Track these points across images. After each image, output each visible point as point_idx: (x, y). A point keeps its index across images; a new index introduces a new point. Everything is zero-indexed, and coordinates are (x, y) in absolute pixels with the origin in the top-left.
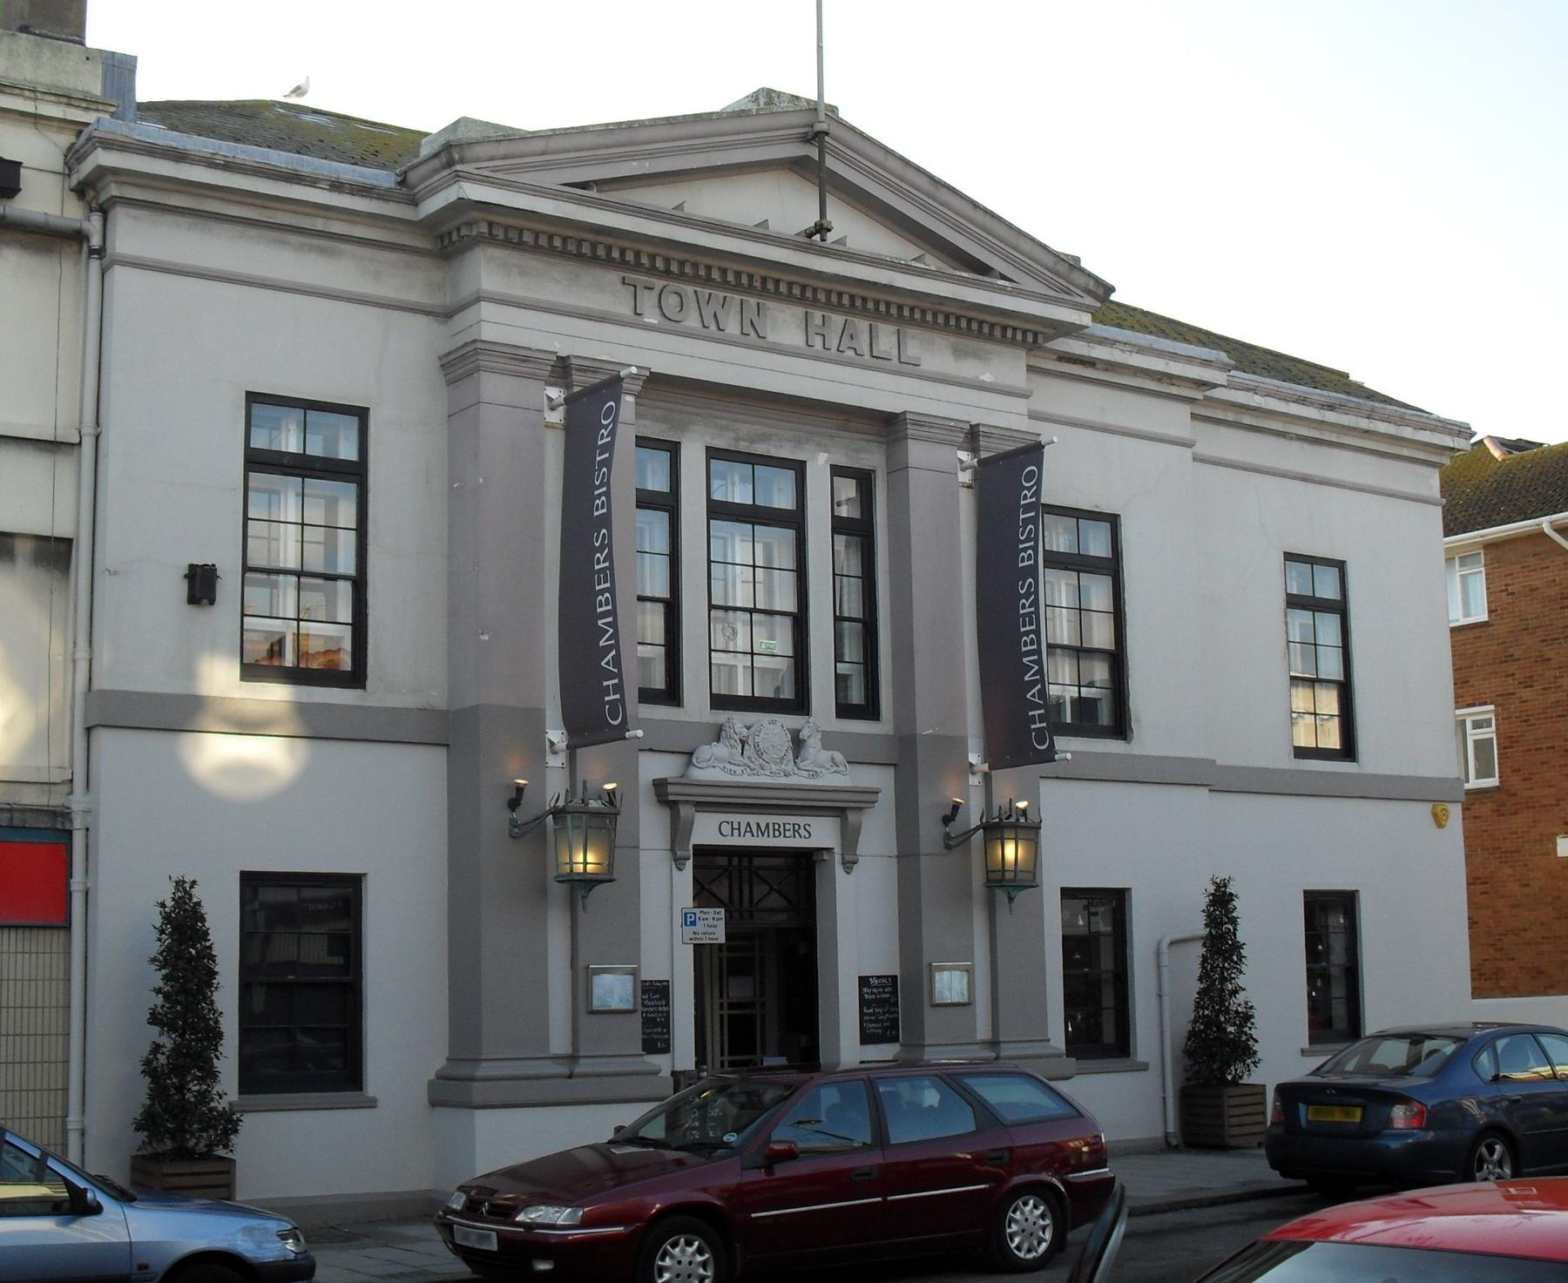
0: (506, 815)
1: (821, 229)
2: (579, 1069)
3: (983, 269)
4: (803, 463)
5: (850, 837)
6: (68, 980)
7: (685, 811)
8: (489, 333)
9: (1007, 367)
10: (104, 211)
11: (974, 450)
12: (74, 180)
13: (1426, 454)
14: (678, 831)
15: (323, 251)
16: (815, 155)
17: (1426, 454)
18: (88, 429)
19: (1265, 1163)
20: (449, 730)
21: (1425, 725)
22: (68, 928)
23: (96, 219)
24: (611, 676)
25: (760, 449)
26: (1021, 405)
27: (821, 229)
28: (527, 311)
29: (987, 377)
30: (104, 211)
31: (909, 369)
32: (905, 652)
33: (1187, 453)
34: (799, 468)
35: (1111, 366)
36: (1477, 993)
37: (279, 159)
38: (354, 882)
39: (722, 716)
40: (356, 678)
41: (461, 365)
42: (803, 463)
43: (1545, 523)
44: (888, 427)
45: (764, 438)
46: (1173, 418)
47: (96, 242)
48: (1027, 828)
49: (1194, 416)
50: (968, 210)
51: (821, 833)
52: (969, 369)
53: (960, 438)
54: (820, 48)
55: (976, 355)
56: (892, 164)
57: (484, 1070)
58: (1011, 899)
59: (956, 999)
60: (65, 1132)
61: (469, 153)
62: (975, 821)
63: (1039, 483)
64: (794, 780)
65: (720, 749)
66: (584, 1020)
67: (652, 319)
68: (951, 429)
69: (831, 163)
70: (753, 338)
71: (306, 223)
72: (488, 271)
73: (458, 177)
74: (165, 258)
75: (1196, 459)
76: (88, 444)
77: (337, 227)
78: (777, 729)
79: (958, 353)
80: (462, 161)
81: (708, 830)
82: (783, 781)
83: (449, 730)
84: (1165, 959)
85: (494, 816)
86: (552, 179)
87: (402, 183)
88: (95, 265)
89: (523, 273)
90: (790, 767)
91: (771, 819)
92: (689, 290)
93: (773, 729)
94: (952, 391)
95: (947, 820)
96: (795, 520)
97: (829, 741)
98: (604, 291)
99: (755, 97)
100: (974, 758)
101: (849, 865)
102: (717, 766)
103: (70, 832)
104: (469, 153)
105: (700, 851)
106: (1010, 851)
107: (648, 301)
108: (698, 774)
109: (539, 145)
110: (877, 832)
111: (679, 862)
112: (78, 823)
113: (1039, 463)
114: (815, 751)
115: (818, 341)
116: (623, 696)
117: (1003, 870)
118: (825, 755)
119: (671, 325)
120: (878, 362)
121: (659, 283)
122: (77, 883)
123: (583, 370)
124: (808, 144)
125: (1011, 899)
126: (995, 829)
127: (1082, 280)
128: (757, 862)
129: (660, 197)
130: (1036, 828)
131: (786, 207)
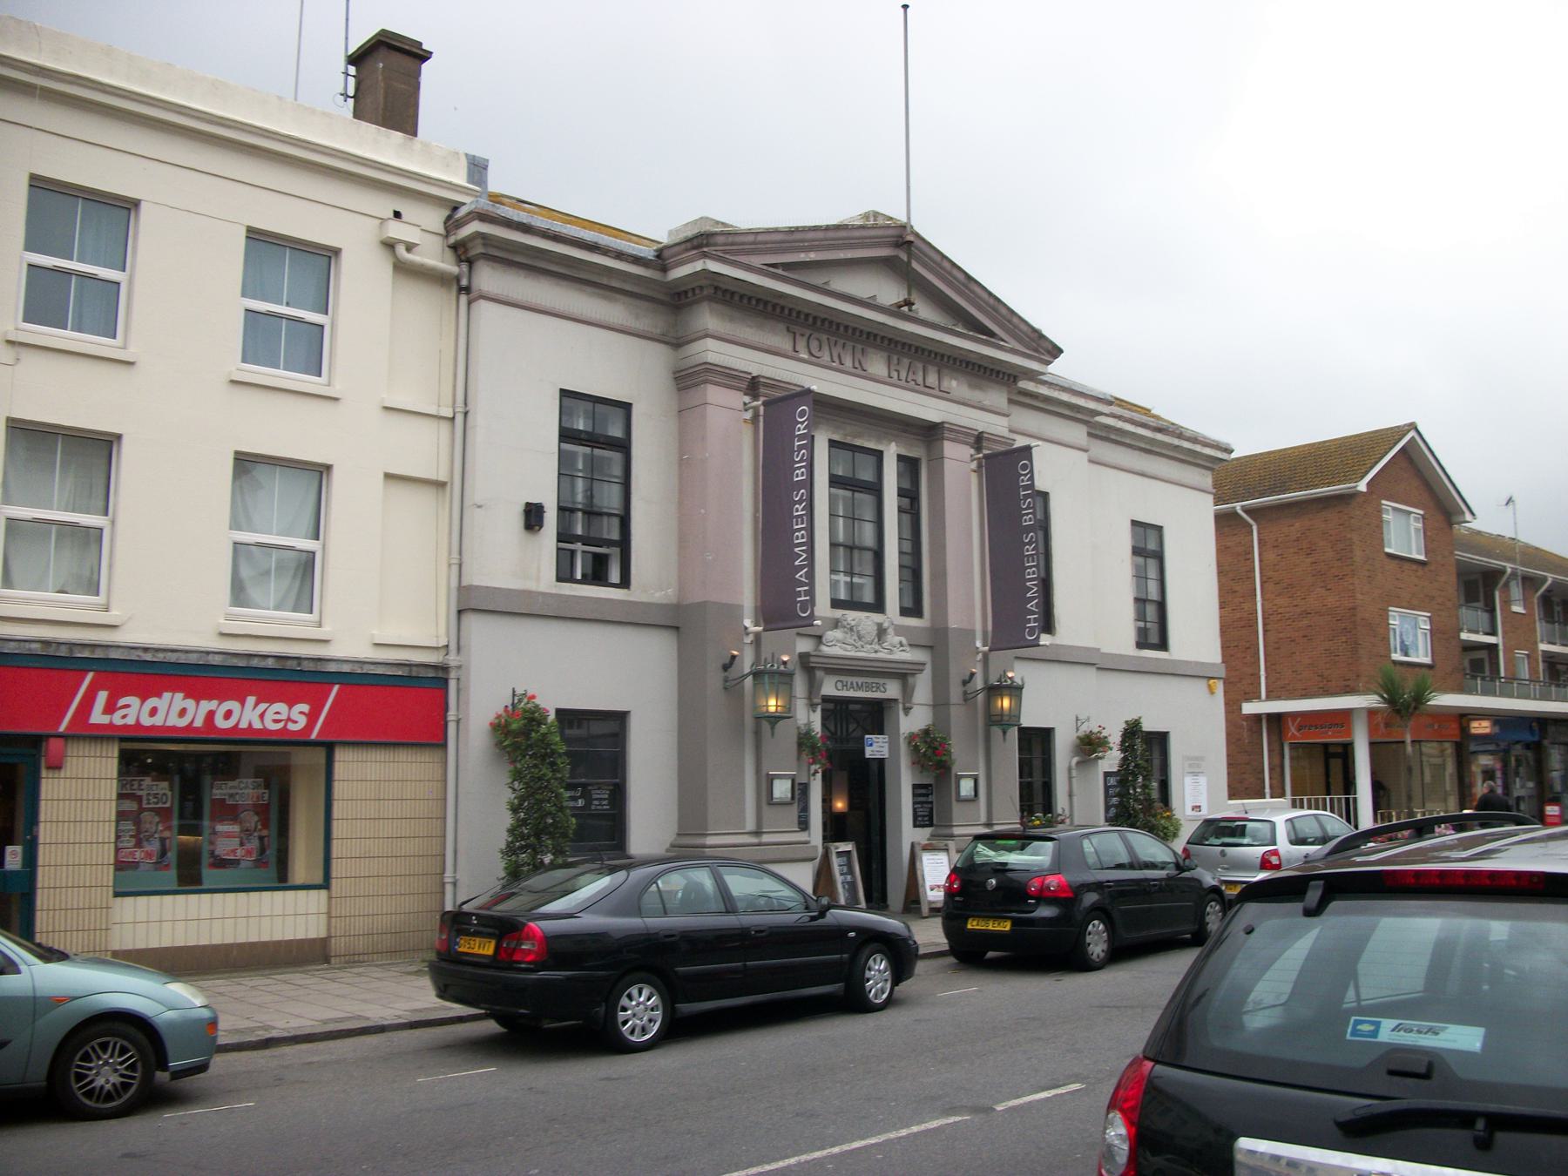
0: (722, 674)
1: (908, 303)
3: (991, 334)
4: (881, 453)
5: (907, 692)
6: (445, 781)
7: (819, 674)
8: (712, 358)
9: (997, 397)
10: (470, 263)
11: (979, 450)
12: (452, 240)
13: (1209, 464)
14: (813, 686)
15: (605, 298)
16: (904, 257)
17: (1209, 464)
18: (460, 408)
20: (677, 621)
21: (1196, 631)
22: (444, 746)
23: (465, 267)
24: (802, 584)
25: (858, 442)
26: (1004, 421)
27: (908, 303)
28: (725, 345)
29: (987, 403)
30: (470, 263)
31: (944, 395)
32: (940, 575)
33: (1085, 456)
34: (879, 455)
35: (1047, 399)
36: (1233, 794)
38: (621, 717)
39: (838, 613)
41: (688, 379)
42: (881, 453)
43: (1238, 506)
44: (930, 433)
45: (859, 436)
46: (1078, 433)
47: (464, 282)
48: (1015, 690)
49: (1090, 434)
50: (985, 296)
51: (892, 690)
53: (972, 440)
55: (980, 388)
56: (946, 265)
57: (710, 841)
58: (1004, 733)
60: (443, 884)
61: (712, 241)
62: (747, 670)
63: (1032, 471)
64: (881, 655)
66: (765, 808)
67: (805, 356)
68: (967, 434)
69: (915, 265)
70: (860, 372)
72: (708, 318)
73: (705, 255)
75: (1091, 461)
76: (459, 419)
77: (615, 284)
79: (972, 386)
80: (707, 245)
81: (830, 688)
82: (873, 655)
83: (677, 621)
84: (1074, 773)
85: (714, 679)
86: (757, 261)
87: (658, 256)
88: (464, 299)
89: (732, 319)
90: (877, 647)
92: (824, 337)
93: (866, 621)
94: (991, 416)
95: (726, 668)
96: (876, 489)
97: (900, 630)
99: (866, 216)
100: (748, 623)
101: (907, 710)
102: (836, 646)
103: (446, 681)
104: (712, 241)
105: (826, 699)
106: (1006, 703)
107: (801, 344)
108: (825, 650)
109: (751, 238)
110: (923, 689)
111: (812, 706)
112: (453, 675)
113: (1030, 459)
114: (892, 639)
115: (895, 374)
116: (578, 582)
117: (1002, 715)
118: (897, 639)
119: (814, 361)
120: (926, 390)
121: (808, 332)
122: (452, 715)
123: (766, 385)
124: (899, 250)
125: (1004, 733)
126: (994, 691)
127: (1047, 345)
128: (852, 707)
129: (817, 279)
130: (1020, 688)
131: (889, 292)
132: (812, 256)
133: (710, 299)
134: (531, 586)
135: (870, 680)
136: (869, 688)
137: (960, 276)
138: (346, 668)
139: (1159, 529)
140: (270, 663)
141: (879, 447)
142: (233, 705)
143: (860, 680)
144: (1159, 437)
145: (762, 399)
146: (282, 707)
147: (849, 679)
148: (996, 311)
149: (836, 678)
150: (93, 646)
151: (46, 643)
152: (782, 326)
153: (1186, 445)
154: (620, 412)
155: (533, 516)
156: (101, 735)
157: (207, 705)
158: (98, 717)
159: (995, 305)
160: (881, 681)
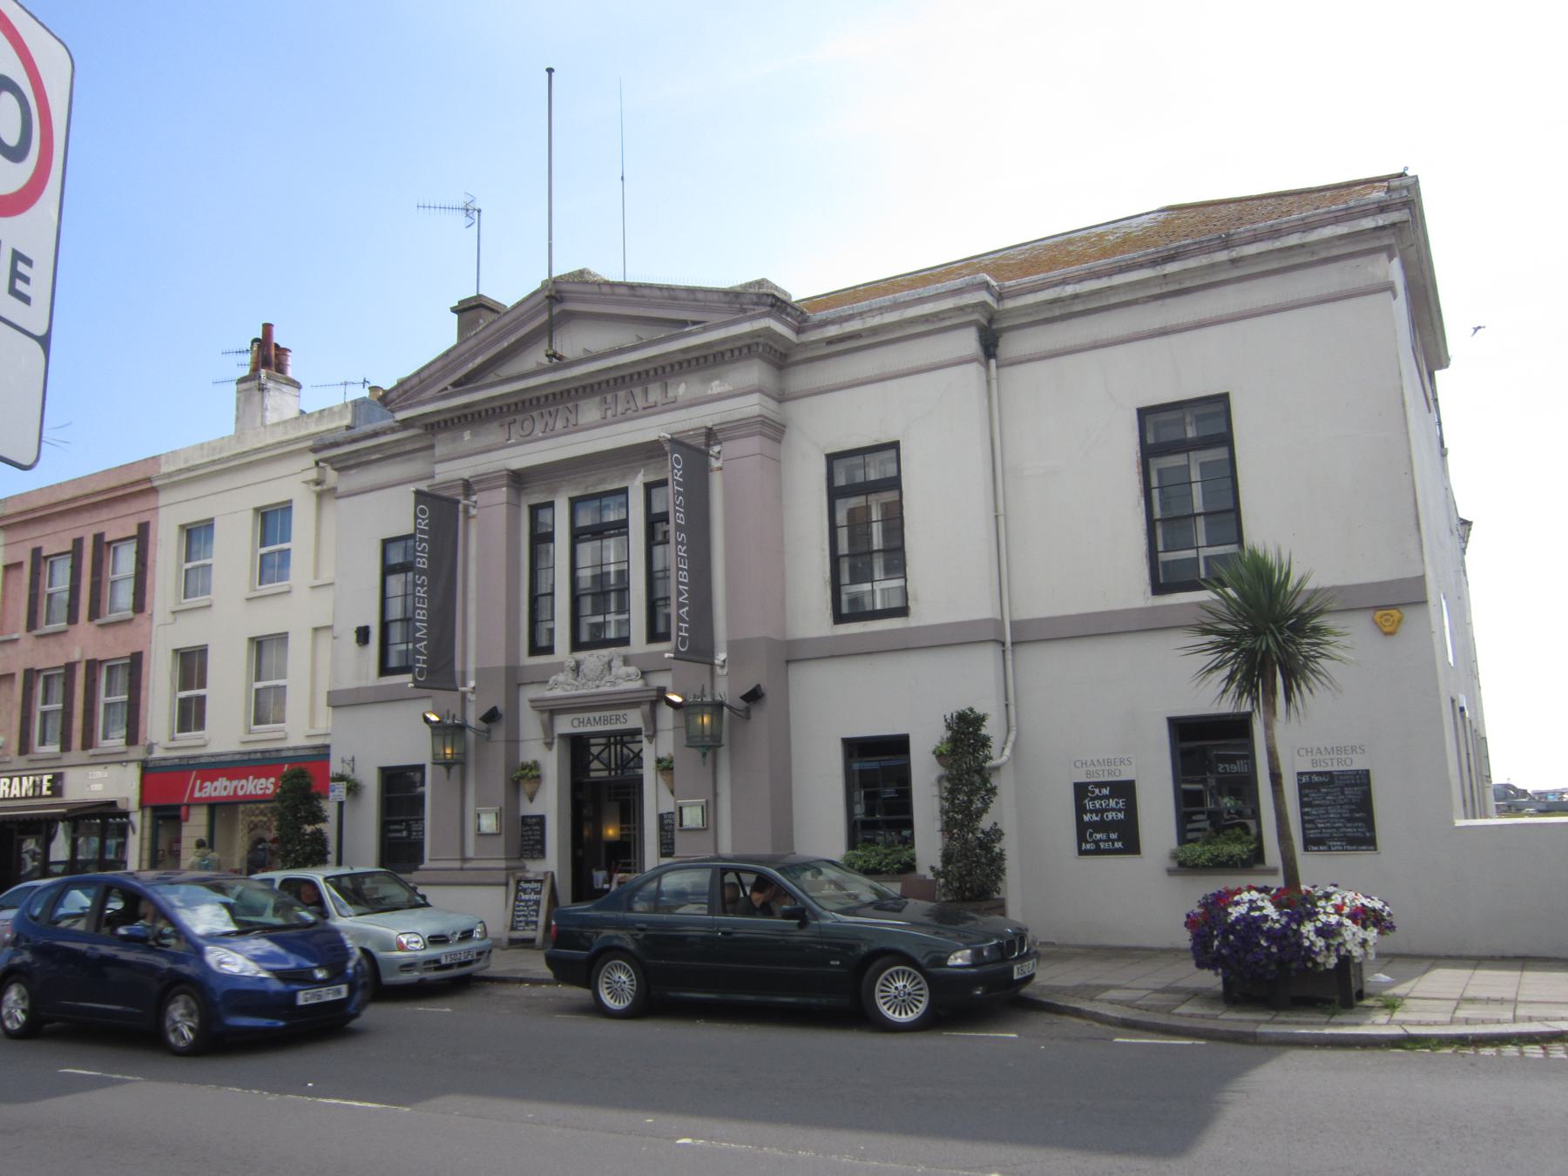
2: (467, 865)
3: (685, 323)
5: (652, 719)
14: (548, 728)
19: (543, 960)
25: (600, 489)
31: (672, 405)
35: (874, 331)
37: (1056, 274)
40: (903, 611)
45: (602, 481)
50: (658, 293)
52: (716, 387)
54: (550, 245)
59: (694, 826)
64: (602, 689)
65: (561, 677)
71: (402, 449)
74: (1231, 310)
78: (593, 659)
81: (565, 725)
82: (574, 693)
91: (602, 714)
98: (493, 434)
101: (652, 737)
105: (562, 736)
109: (415, 381)
111: (549, 745)
120: (651, 410)
129: (491, 378)
132: (479, 360)
133: (761, 356)
134: (363, 684)
135: (608, 713)
136: (607, 721)
137: (624, 291)
138: (291, 753)
139: (386, 543)
140: (259, 756)
141: (623, 485)
142: (243, 782)
143: (597, 715)
144: (1170, 268)
145: (461, 498)
146: (263, 780)
147: (586, 715)
148: (675, 299)
149: (571, 716)
150: (195, 757)
151: (180, 758)
152: (495, 425)
153: (1294, 240)
154: (1150, 420)
155: (363, 635)
156: (199, 802)
157: (235, 783)
158: (197, 795)
159: (670, 294)
160: (621, 712)
